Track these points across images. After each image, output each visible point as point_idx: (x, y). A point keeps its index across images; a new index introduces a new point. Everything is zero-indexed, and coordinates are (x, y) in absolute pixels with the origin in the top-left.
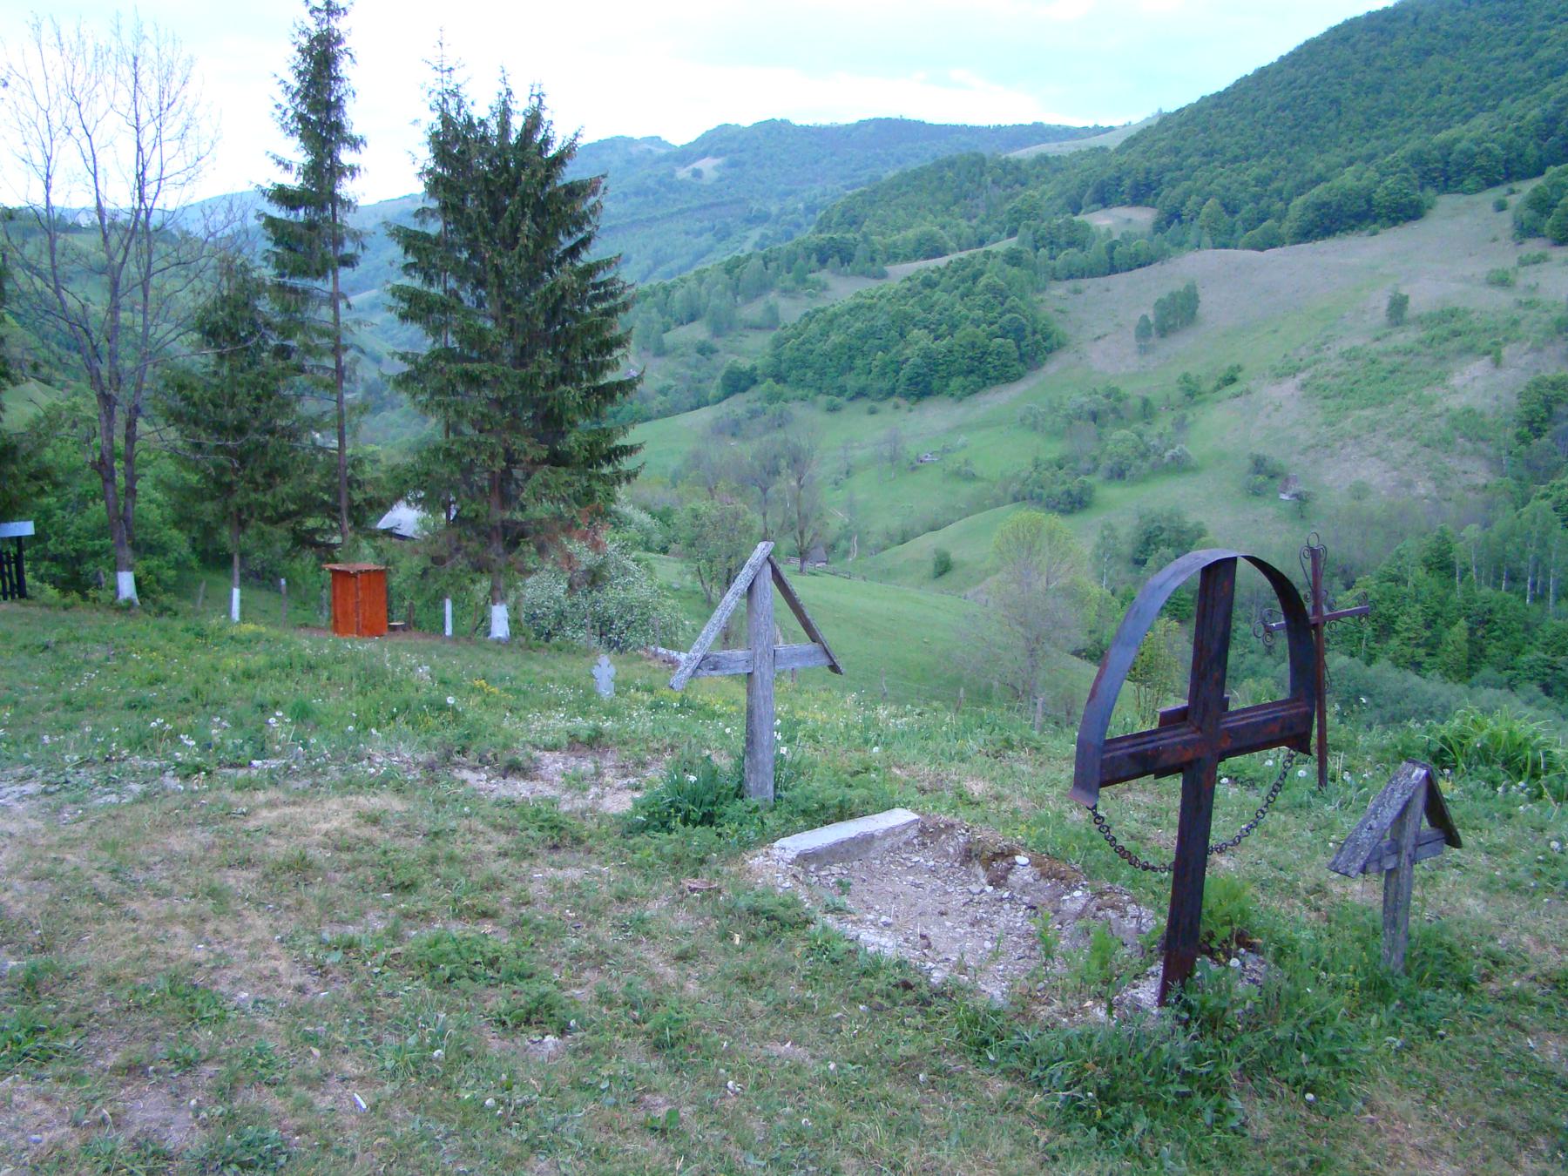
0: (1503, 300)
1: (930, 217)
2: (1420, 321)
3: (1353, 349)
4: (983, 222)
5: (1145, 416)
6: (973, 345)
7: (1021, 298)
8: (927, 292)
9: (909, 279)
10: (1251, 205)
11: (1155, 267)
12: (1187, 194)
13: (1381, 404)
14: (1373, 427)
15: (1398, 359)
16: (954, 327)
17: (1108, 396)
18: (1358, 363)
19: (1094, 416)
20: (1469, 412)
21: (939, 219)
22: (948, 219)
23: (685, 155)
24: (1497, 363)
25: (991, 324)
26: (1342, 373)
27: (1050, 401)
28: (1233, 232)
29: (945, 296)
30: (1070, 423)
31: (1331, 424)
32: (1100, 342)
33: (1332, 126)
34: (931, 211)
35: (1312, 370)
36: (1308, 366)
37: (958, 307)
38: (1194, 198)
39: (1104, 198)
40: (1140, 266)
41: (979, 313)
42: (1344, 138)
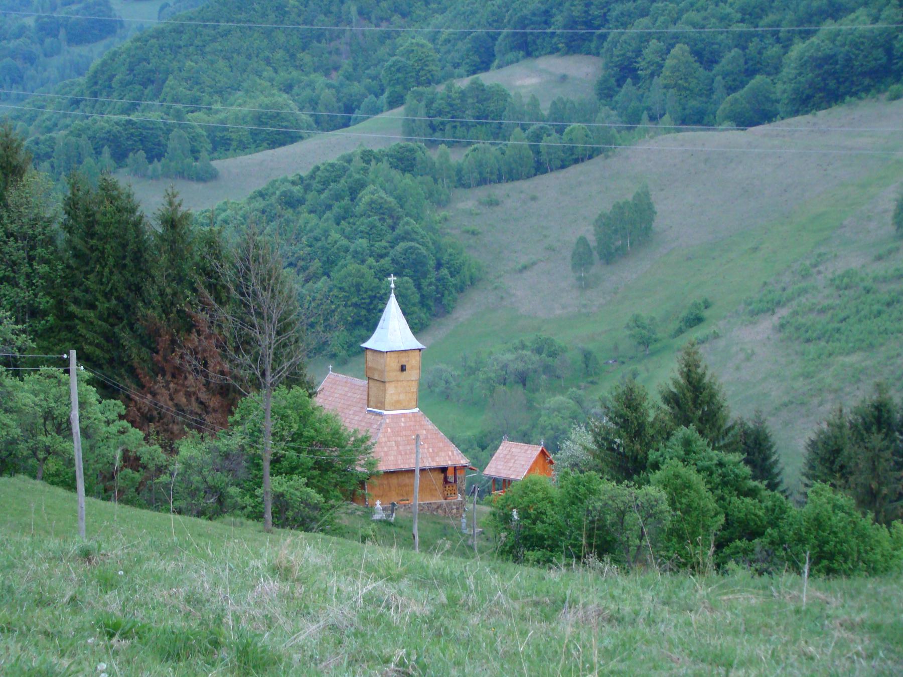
1: (268, 72)
3: (848, 274)
4: (348, 77)
5: (588, 374)
6: (358, 286)
7: (418, 218)
8: (289, 213)
9: (262, 195)
10: (735, 52)
11: (598, 160)
13: (871, 346)
16: (330, 263)
17: (539, 351)
19: (523, 379)
21: (283, 75)
22: (295, 74)
25: (382, 256)
26: (830, 308)
27: (465, 359)
28: (711, 91)
29: (313, 219)
30: (492, 390)
32: (527, 274)
34: (268, 61)
35: (795, 303)
36: (789, 300)
38: (653, 43)
40: (576, 161)
41: (362, 243)
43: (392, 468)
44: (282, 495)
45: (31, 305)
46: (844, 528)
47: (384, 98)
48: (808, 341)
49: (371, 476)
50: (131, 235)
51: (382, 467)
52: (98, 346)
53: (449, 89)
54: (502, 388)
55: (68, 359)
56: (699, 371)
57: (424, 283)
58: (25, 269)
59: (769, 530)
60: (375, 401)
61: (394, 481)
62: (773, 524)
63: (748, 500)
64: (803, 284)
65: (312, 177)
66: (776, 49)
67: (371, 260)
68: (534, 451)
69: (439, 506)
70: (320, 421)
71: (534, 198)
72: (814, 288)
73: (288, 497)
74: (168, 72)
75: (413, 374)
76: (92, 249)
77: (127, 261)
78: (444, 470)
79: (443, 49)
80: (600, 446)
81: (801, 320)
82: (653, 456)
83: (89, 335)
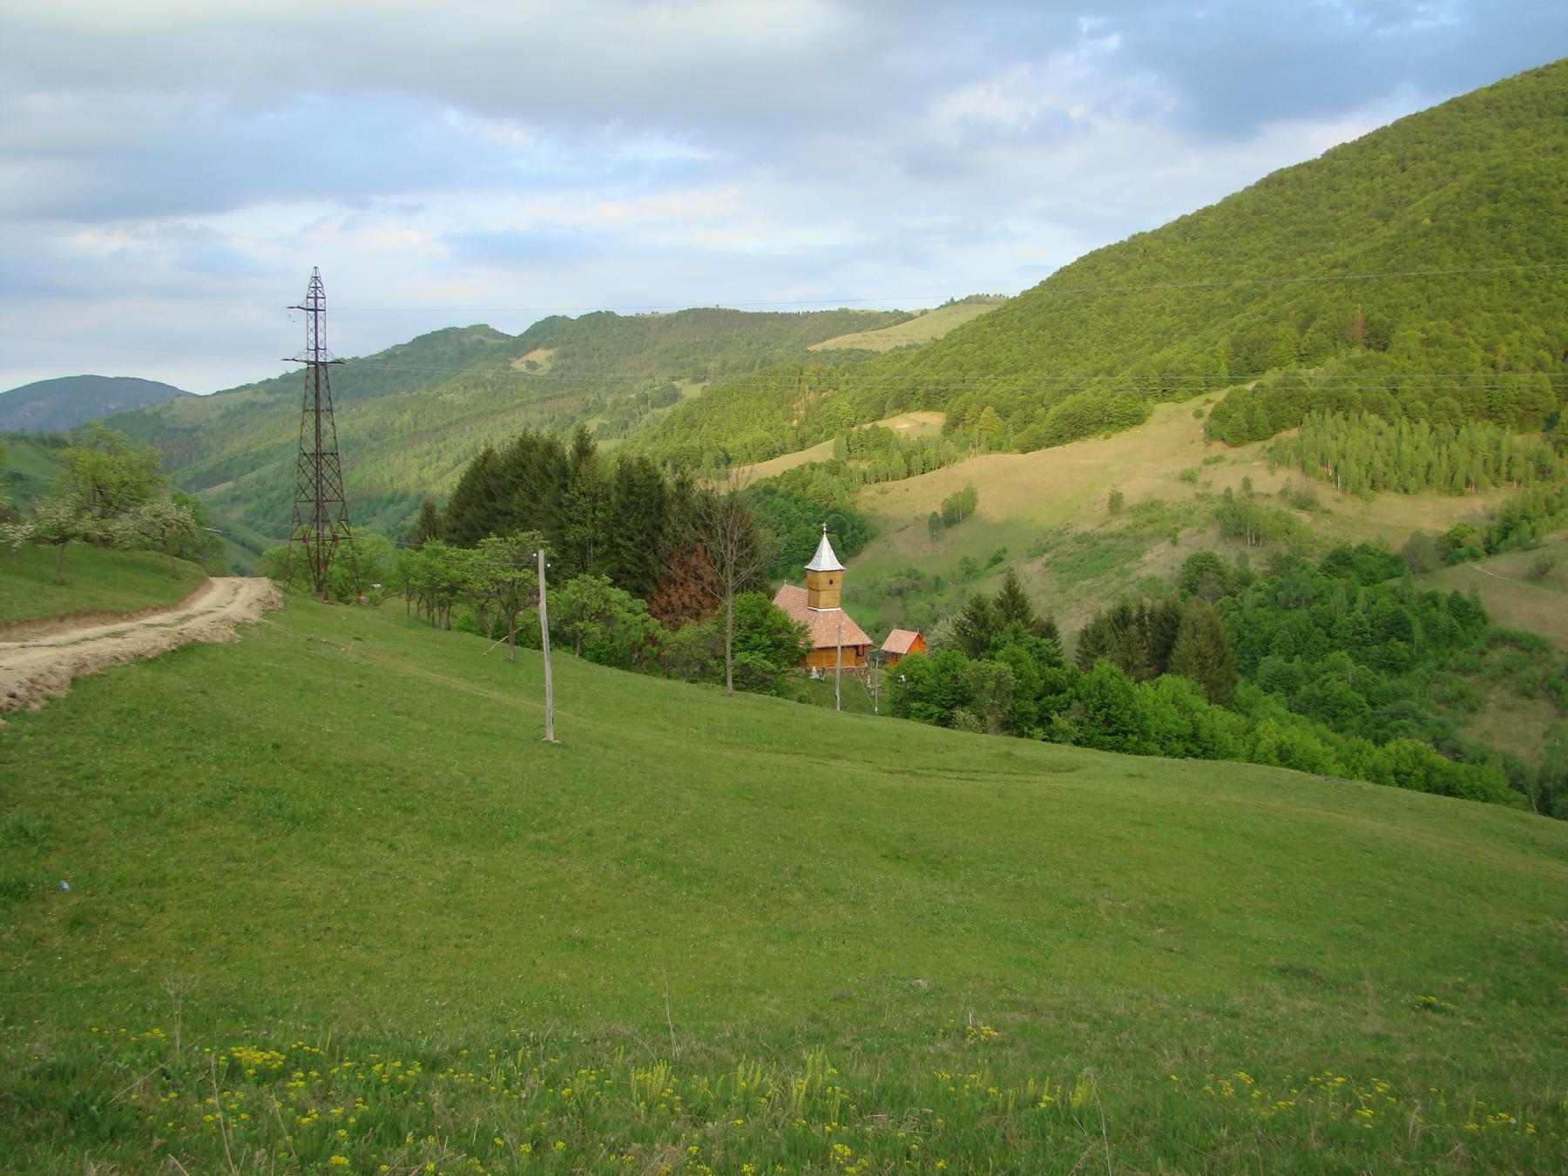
0: (1188, 492)
2: (1131, 510)
6: (807, 539)
8: (768, 498)
12: (969, 402)
14: (1089, 592)
15: (1112, 541)
16: (791, 526)
17: (909, 577)
18: (1085, 545)
19: (900, 592)
20: (1152, 579)
23: (519, 346)
24: (1174, 543)
26: (1074, 553)
31: (1062, 592)
33: (1081, 342)
37: (794, 510)
39: (903, 404)
42: (1092, 352)
43: (823, 646)
44: (747, 664)
45: (594, 539)
46: (1117, 688)
47: (823, 435)
48: (1062, 572)
49: (808, 651)
50: (656, 493)
51: (817, 645)
52: (634, 564)
53: (859, 429)
54: (888, 597)
55: (537, 558)
56: (1016, 586)
57: (845, 537)
58: (590, 515)
59: (1069, 689)
60: (813, 603)
61: (824, 654)
62: (1072, 685)
63: (1056, 669)
64: (1059, 540)
65: (782, 477)
66: (1042, 410)
67: (814, 525)
68: (913, 636)
69: (853, 670)
70: (775, 615)
71: (907, 490)
72: (1066, 543)
73: (751, 666)
74: (704, 421)
75: (837, 586)
76: (632, 502)
77: (653, 510)
78: (856, 647)
79: (856, 408)
80: (959, 633)
81: (1060, 560)
82: (993, 639)
83: (629, 558)
